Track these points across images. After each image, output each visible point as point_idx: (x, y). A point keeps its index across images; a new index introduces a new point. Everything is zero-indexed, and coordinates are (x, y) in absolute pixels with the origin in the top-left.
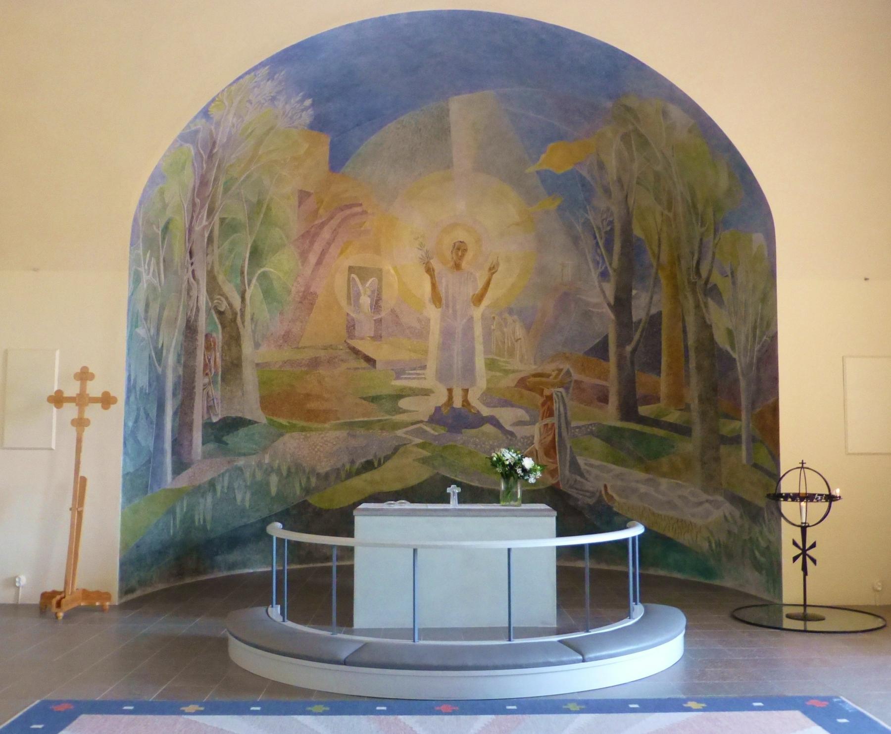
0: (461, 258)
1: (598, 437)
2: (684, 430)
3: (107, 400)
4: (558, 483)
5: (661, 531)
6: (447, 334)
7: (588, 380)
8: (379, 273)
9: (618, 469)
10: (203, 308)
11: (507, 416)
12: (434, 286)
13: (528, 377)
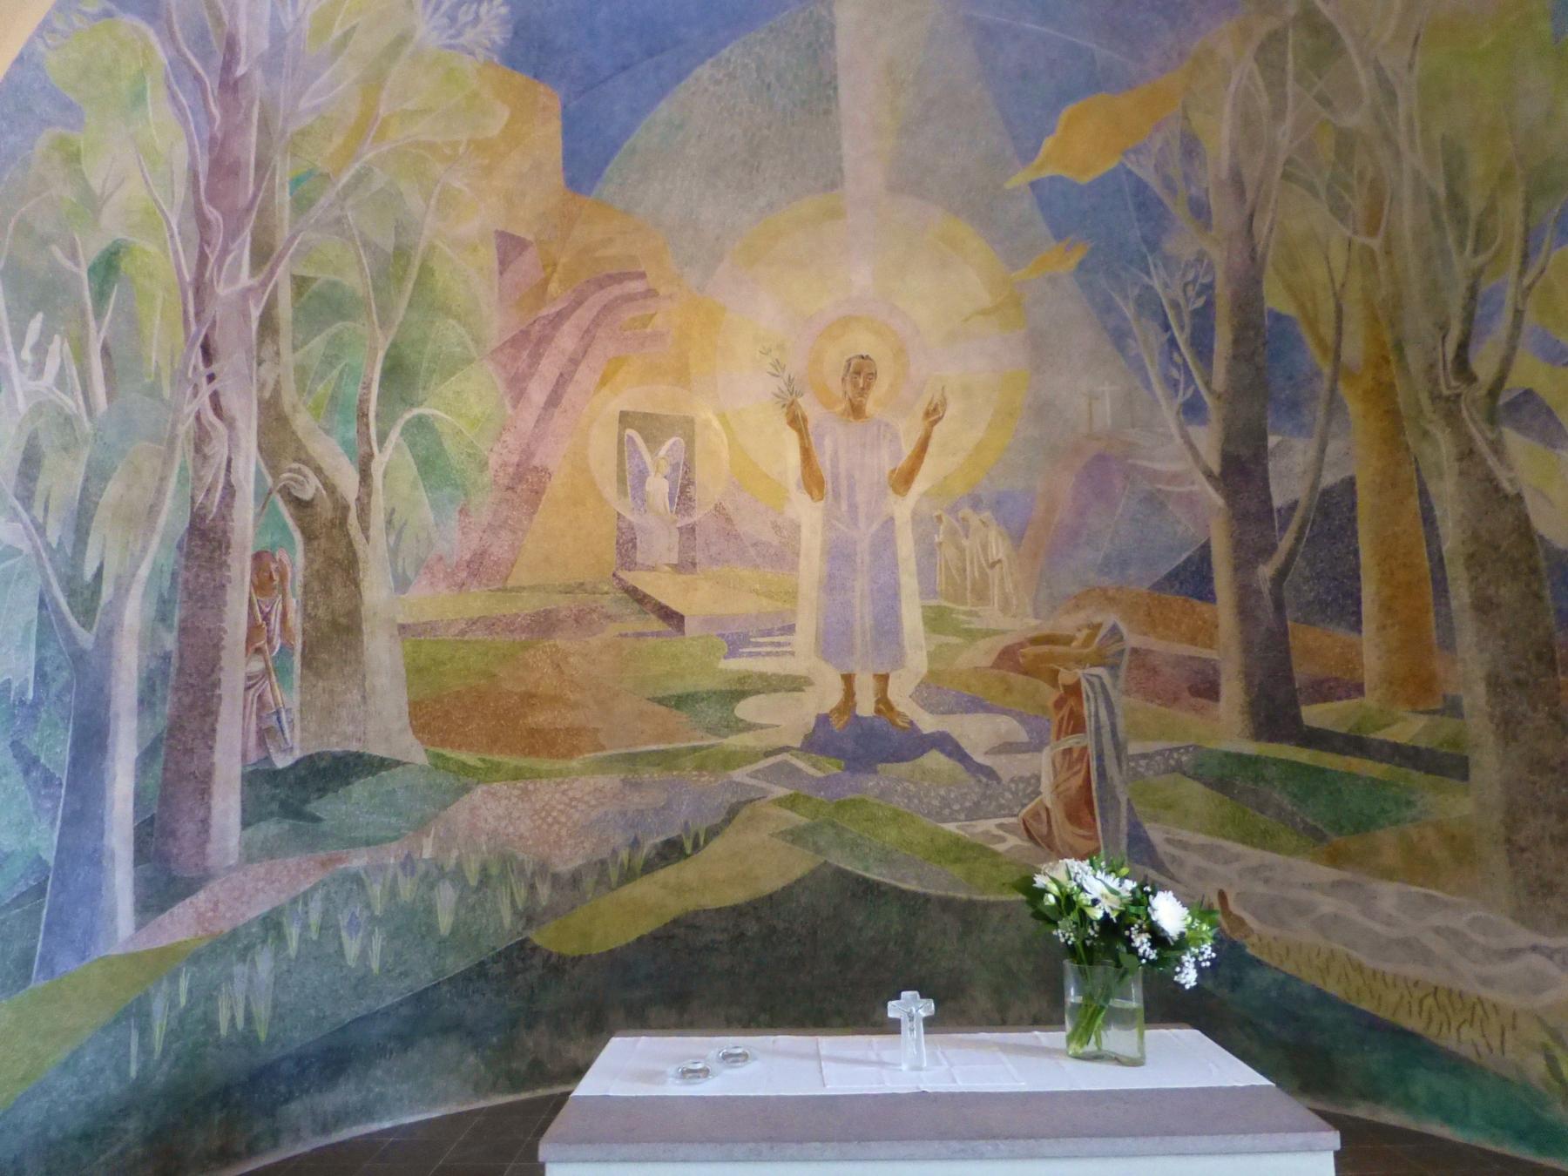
0: (864, 391)
1: (1196, 777)
2: (1448, 764)
5: (1384, 1014)
6: (838, 555)
7: (1166, 647)
8: (687, 428)
9: (1255, 856)
12: (806, 454)
13: (1021, 645)
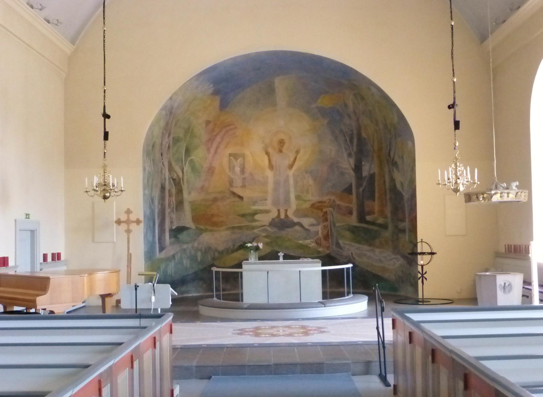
0: (282, 147)
2: (384, 227)
3: (138, 222)
4: (330, 253)
6: (277, 184)
7: (343, 204)
8: (243, 156)
9: (357, 245)
10: (167, 178)
11: (306, 222)
12: (270, 160)
